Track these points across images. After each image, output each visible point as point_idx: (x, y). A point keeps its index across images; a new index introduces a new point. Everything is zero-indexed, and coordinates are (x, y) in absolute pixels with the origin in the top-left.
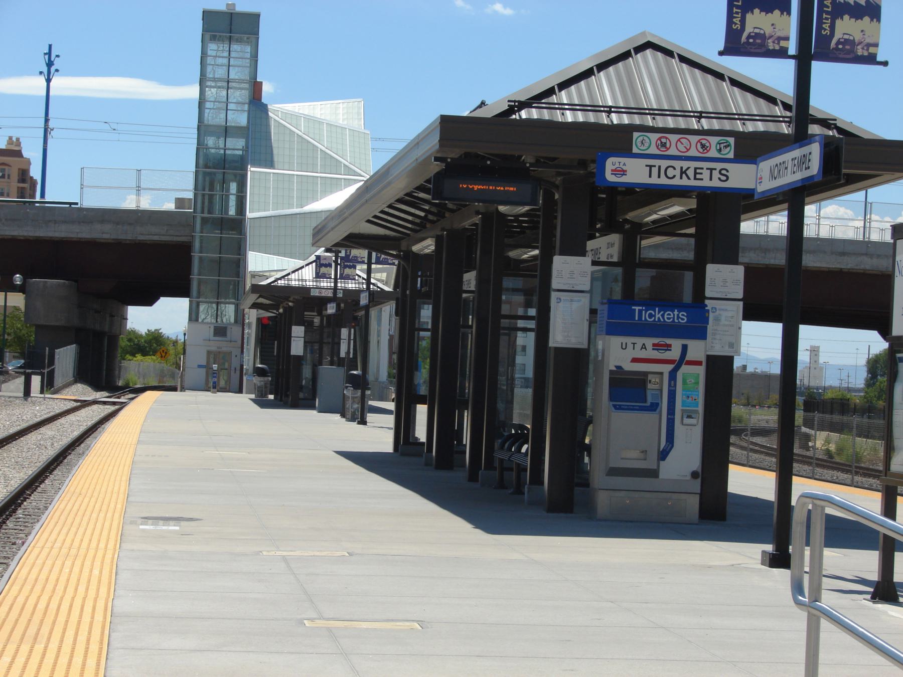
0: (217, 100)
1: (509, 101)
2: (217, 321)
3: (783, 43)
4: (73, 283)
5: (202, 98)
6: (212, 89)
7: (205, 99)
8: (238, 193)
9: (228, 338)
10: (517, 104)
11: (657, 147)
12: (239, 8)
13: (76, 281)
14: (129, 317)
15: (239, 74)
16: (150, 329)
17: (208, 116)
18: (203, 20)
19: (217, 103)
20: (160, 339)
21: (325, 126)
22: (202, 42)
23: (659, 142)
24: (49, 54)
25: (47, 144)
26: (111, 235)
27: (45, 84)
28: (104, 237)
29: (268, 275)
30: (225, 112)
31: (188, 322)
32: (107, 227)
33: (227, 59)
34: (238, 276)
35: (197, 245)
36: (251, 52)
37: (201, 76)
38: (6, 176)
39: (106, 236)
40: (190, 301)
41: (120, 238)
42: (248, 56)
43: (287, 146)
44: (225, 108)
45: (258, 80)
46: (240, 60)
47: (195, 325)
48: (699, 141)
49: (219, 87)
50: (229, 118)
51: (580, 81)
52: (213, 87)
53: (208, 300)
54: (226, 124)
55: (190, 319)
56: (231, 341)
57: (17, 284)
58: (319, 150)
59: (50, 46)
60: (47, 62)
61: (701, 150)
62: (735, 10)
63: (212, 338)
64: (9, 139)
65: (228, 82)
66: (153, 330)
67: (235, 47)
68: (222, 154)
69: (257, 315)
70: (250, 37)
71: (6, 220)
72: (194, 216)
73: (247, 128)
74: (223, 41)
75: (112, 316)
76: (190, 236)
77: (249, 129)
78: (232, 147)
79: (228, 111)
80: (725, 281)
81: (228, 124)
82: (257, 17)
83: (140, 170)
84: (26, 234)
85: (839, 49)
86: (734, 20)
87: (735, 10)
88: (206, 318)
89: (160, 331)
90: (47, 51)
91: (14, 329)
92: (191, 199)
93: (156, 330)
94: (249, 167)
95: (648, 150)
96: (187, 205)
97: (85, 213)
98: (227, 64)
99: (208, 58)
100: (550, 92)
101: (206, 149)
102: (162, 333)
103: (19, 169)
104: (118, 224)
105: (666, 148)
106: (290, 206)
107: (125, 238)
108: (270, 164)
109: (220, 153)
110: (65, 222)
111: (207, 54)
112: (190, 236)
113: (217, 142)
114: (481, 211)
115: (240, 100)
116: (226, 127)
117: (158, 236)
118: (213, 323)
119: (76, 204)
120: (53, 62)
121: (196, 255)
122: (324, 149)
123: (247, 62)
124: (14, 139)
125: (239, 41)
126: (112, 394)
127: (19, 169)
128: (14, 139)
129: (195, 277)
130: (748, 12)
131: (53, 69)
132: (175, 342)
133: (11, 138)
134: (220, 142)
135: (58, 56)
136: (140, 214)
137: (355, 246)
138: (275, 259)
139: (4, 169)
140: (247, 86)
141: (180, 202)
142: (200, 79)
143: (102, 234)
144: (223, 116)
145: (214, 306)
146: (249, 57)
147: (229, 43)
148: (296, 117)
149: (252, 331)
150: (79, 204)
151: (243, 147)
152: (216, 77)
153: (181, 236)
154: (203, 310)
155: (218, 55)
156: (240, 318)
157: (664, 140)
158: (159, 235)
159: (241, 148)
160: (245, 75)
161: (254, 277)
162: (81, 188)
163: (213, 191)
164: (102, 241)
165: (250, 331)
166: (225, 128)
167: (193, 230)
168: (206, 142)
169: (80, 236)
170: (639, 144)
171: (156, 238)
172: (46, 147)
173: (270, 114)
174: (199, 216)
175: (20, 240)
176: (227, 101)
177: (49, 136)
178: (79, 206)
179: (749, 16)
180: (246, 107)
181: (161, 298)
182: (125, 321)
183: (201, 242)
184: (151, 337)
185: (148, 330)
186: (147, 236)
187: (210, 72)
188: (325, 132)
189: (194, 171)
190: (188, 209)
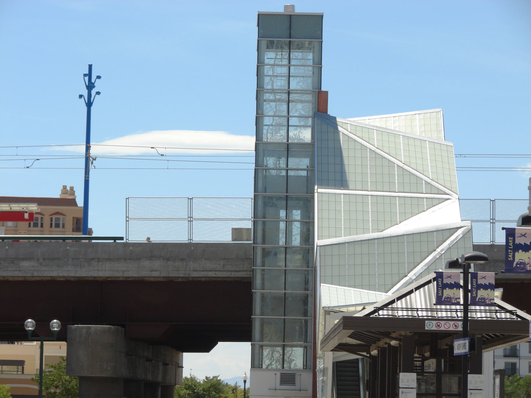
0: (277, 114)
1: (374, 308)
2: (283, 367)
3: (458, 300)
4: (120, 328)
5: (260, 113)
6: (271, 103)
7: (263, 114)
8: (304, 219)
9: (297, 387)
10: (377, 309)
11: (436, 327)
12: (299, 10)
13: (123, 326)
14: (184, 365)
15: (301, 84)
16: (208, 376)
17: (267, 133)
18: (258, 25)
19: (277, 118)
20: (215, 383)
21: (401, 138)
22: (257, 75)
23: (436, 324)
24: (90, 75)
25: (89, 175)
26: (160, 273)
27: (86, 108)
28: (153, 275)
29: (346, 311)
30: (286, 128)
31: (251, 370)
32: (157, 264)
33: (287, 68)
34: (305, 314)
35: (258, 281)
36: (313, 58)
37: (258, 63)
38: (61, 225)
39: (156, 274)
40: (252, 344)
41: (171, 275)
42: (311, 63)
43: (359, 162)
44: (286, 124)
45: (323, 89)
46: (302, 67)
47: (258, 373)
48: (454, 324)
49: (279, 100)
50: (291, 134)
51: (420, 288)
52: (271, 101)
53: (272, 343)
54: (288, 141)
55: (253, 366)
56: (300, 390)
57: (55, 331)
58: (396, 165)
59: (90, 67)
60: (87, 85)
61: (455, 328)
62: (439, 289)
63: (278, 386)
64: (63, 188)
65: (289, 93)
66: (211, 377)
67: (296, 55)
68: (283, 176)
69: (333, 358)
70: (312, 41)
71: (44, 259)
72: (254, 247)
73: (312, 144)
74: (282, 48)
75: (165, 364)
76: (250, 271)
77: (314, 147)
78: (295, 167)
79: (290, 127)
80: (476, 382)
81: (290, 141)
82: (319, 18)
83: (192, 199)
84: (66, 274)
85: (480, 301)
86: (439, 292)
87: (439, 289)
88: (271, 364)
89: (218, 379)
90: (87, 72)
91: (62, 381)
92: (250, 229)
93: (214, 377)
94: (316, 187)
95: (433, 328)
96: (245, 237)
97: (131, 248)
98: (287, 75)
99: (266, 67)
100: (393, 302)
101: (266, 170)
102: (220, 380)
103: (73, 218)
104: (168, 260)
105: (440, 327)
106: (365, 230)
107: (177, 275)
108: (342, 183)
109: (282, 174)
110: (109, 260)
111: (264, 63)
112: (250, 271)
113: (278, 162)
114: (387, 342)
115: (303, 113)
116: (288, 144)
117: (214, 273)
118: (279, 370)
119: (122, 238)
120: (94, 84)
121: (257, 292)
122: (401, 164)
123: (309, 71)
124: (68, 188)
125: (300, 47)
126: (501, 310)
127: (73, 218)
128: (68, 188)
129: (257, 318)
130: (444, 289)
131: (93, 92)
132: (235, 389)
133: (65, 187)
134: (281, 162)
135: (99, 77)
136: (192, 248)
137: (340, 350)
138: (352, 292)
139: (59, 219)
140: (309, 97)
141: (237, 233)
142: (257, 91)
143: (151, 271)
144: (283, 132)
145: (280, 349)
146: (311, 64)
147: (288, 50)
148: (369, 129)
149: (327, 378)
150: (125, 239)
151: (308, 167)
152: (275, 88)
153: (240, 271)
154: (268, 354)
155: (276, 63)
156: (310, 363)
157: (438, 324)
158: (215, 271)
159: (306, 167)
160: (307, 84)
161: (329, 314)
162: (126, 221)
163: (264, 267)
164: (152, 279)
165: (325, 378)
166: (286, 146)
167: (254, 264)
168: (265, 162)
169: (126, 275)
170: (428, 326)
171: (211, 274)
172: (88, 177)
173: (340, 129)
174: (259, 247)
175: (60, 281)
176: (288, 115)
177: (91, 167)
178: (124, 241)
179: (444, 291)
180: (310, 121)
181: (219, 342)
182: (180, 369)
183: (263, 275)
184: (209, 385)
185: (207, 378)
186: (202, 273)
187: (268, 83)
188: (402, 145)
189: (253, 196)
190: (247, 240)
